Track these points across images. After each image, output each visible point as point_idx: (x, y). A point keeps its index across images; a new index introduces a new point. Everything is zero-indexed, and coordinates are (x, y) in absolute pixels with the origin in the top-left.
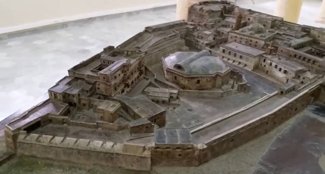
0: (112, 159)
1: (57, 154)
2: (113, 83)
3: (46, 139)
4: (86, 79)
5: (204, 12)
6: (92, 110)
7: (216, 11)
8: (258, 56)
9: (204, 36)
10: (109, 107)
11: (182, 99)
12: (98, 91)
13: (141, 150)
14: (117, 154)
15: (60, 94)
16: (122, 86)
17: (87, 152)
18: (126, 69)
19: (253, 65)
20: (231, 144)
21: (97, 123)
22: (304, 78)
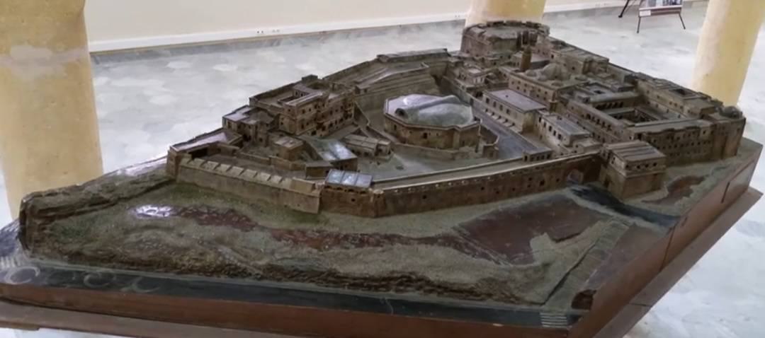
0: (278, 195)
1: (220, 183)
2: (299, 117)
3: (211, 165)
4: (269, 110)
5: (485, 39)
6: (268, 148)
7: (506, 40)
8: (531, 111)
9: (468, 76)
10: (285, 143)
11: (395, 156)
12: (281, 128)
13: (309, 188)
14: (284, 190)
15: (235, 122)
16: (314, 126)
17: (253, 185)
18: (320, 104)
19: (521, 124)
20: (424, 203)
21: (270, 158)
22: (577, 146)
